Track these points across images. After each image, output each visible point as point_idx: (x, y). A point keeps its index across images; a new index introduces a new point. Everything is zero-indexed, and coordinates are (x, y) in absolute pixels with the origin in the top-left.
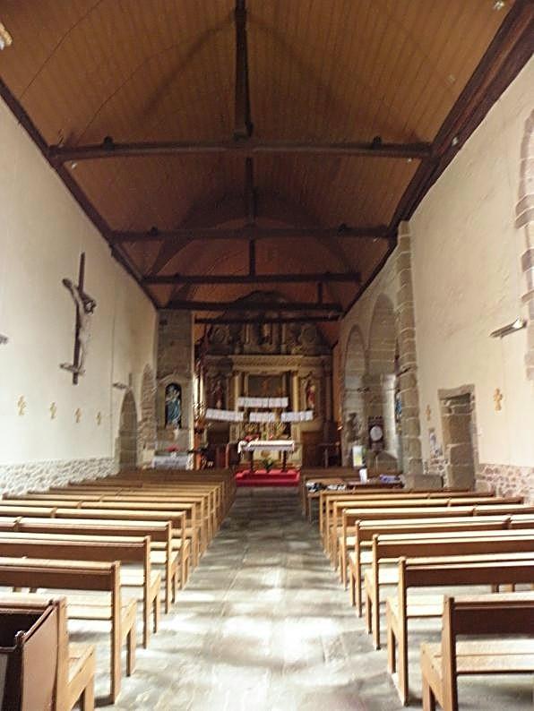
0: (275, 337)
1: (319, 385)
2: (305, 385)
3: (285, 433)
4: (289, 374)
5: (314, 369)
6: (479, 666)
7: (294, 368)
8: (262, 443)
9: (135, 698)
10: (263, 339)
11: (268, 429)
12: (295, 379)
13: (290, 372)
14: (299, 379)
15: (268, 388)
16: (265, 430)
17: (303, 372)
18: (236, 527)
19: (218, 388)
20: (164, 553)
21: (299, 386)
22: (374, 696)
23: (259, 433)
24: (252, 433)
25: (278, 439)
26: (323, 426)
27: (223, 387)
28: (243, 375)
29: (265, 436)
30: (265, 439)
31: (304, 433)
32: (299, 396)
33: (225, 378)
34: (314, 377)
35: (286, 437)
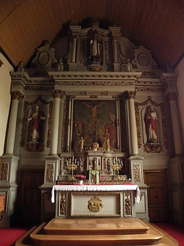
0: (106, 58)
1: (160, 112)
2: (144, 112)
3: (121, 173)
4: (126, 96)
5: (152, 94)
6: (49, 228)
7: (131, 89)
8: (91, 188)
9: (107, 36)
10: (93, 58)
11: (98, 167)
12: (132, 101)
13: (126, 93)
14: (136, 105)
15: (98, 116)
16: (93, 168)
17: (141, 96)
18: (25, 100)
19: (36, 115)
20: (130, 70)
21: (137, 113)
22: (38, 226)
23: (86, 173)
24: (76, 172)
25: (113, 181)
26: (169, 163)
27: (42, 113)
28: (68, 98)
29: (94, 177)
30: (95, 183)
31: (146, 173)
32: (138, 125)
33: (46, 103)
34: (153, 103)
35: (124, 178)
